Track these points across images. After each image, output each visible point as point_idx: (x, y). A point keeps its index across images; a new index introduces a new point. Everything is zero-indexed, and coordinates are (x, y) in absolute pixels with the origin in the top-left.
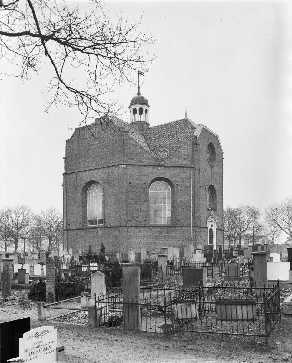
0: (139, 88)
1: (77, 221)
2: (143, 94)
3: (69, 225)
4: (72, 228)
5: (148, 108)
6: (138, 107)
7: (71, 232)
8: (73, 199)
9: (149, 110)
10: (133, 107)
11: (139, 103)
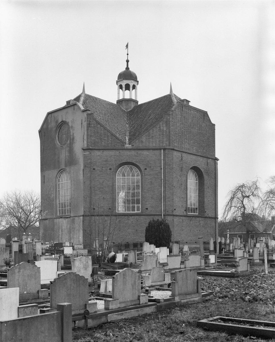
0: (128, 61)
1: (182, 206)
2: (131, 69)
3: (175, 209)
4: (178, 214)
5: (137, 83)
6: (124, 83)
7: (177, 218)
8: (179, 180)
9: (138, 87)
10: (119, 84)
11: (127, 79)
